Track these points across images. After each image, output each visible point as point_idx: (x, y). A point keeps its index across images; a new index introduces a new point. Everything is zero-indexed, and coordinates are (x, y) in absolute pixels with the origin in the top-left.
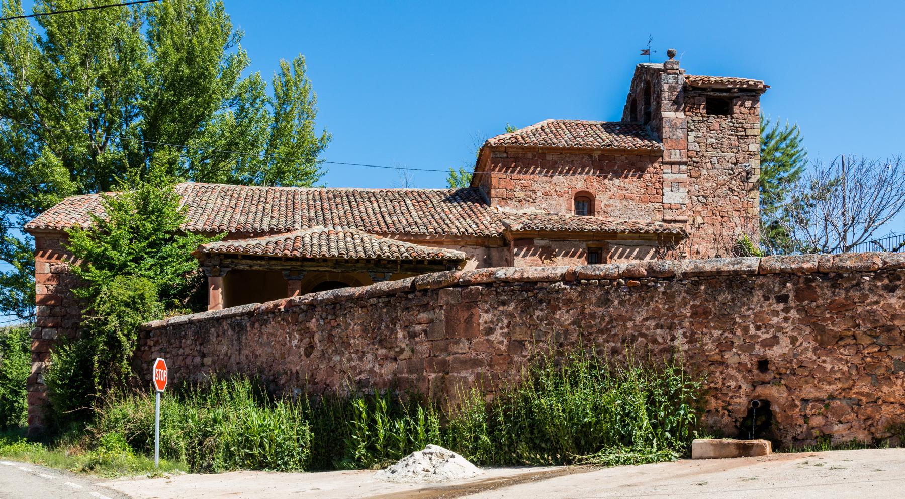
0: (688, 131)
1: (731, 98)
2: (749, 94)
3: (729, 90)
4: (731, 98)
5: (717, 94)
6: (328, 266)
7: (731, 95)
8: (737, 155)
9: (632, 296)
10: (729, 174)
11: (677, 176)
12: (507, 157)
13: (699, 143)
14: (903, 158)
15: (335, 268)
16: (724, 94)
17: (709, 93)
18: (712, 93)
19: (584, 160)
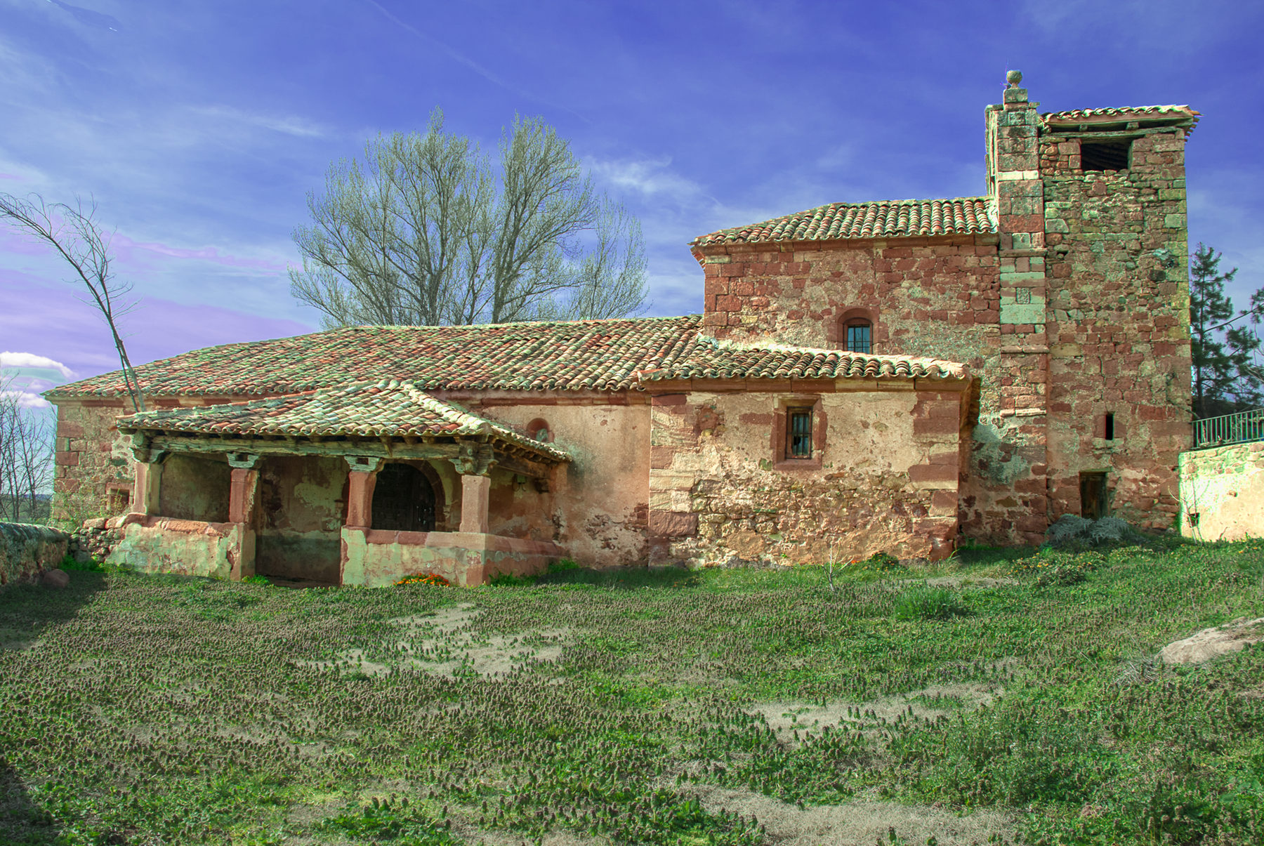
0: (1044, 201)
1: (1130, 140)
2: (1163, 129)
3: (1122, 127)
4: (1130, 140)
5: (1102, 134)
6: (287, 447)
7: (1127, 134)
8: (1141, 236)
9: (968, 344)
10: (1127, 269)
11: (1027, 276)
12: (731, 262)
13: (1066, 220)
14: (1260, 345)
15: (298, 450)
16: (1115, 134)
17: (1085, 135)
18: (1091, 135)
19: (858, 259)
